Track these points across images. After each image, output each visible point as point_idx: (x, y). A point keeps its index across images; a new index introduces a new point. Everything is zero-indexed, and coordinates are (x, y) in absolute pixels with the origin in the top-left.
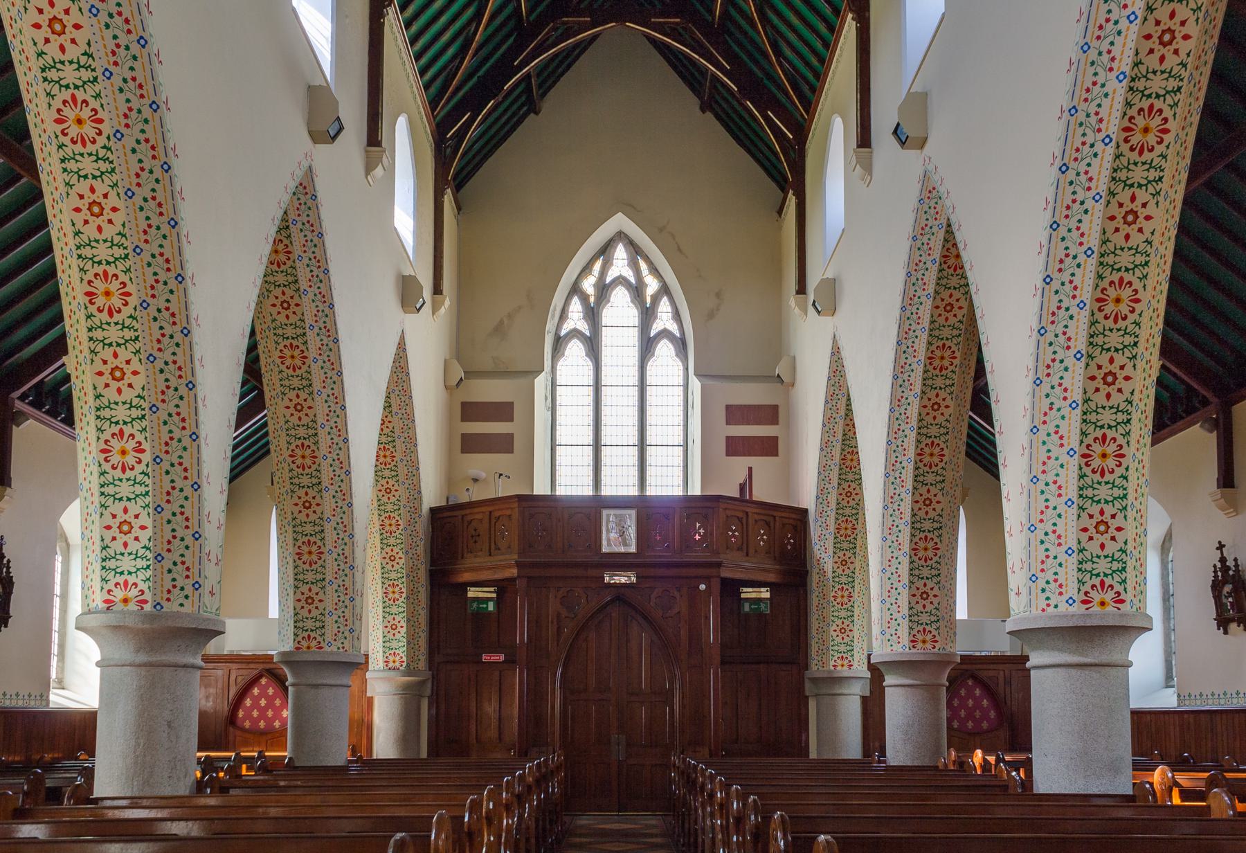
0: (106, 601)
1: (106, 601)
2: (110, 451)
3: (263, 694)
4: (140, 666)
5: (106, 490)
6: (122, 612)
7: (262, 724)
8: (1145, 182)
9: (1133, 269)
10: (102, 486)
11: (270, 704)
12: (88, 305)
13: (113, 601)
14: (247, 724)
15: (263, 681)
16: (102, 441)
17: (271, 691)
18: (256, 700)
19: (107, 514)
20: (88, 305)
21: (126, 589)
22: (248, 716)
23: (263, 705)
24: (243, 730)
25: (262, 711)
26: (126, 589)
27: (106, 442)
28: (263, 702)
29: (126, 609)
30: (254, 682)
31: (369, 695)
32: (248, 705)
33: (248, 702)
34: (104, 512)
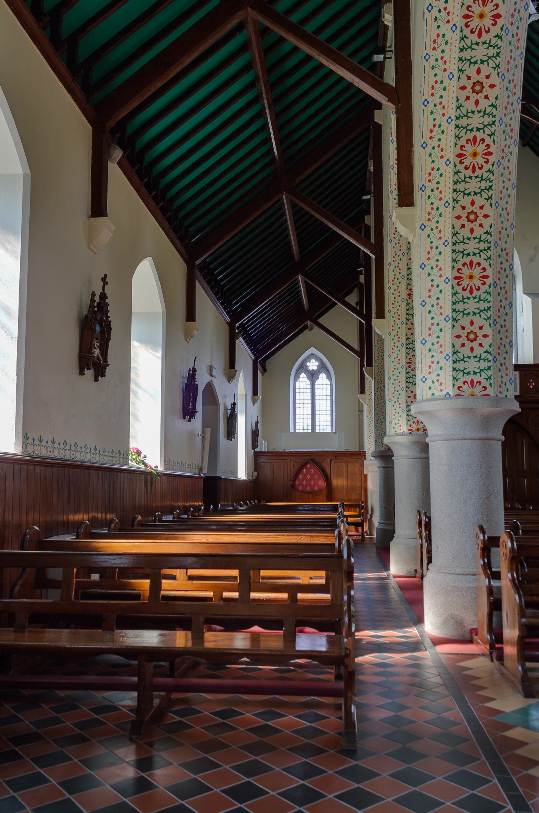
0: (409, 430)
1: (409, 430)
2: (411, 363)
3: (308, 472)
4: (423, 459)
5: (409, 380)
6: (417, 434)
7: (308, 488)
8: (486, 58)
9: (483, 129)
10: (407, 378)
11: (312, 478)
12: (408, 299)
13: (412, 430)
14: (301, 488)
15: (308, 466)
16: (408, 358)
17: (312, 471)
18: (305, 476)
19: (409, 391)
20: (408, 299)
21: (418, 424)
22: (301, 484)
23: (308, 478)
24: (299, 491)
25: (308, 481)
26: (418, 424)
27: (410, 359)
28: (308, 477)
29: (418, 433)
30: (303, 466)
31: (365, 473)
32: (301, 478)
33: (301, 477)
34: (408, 390)
